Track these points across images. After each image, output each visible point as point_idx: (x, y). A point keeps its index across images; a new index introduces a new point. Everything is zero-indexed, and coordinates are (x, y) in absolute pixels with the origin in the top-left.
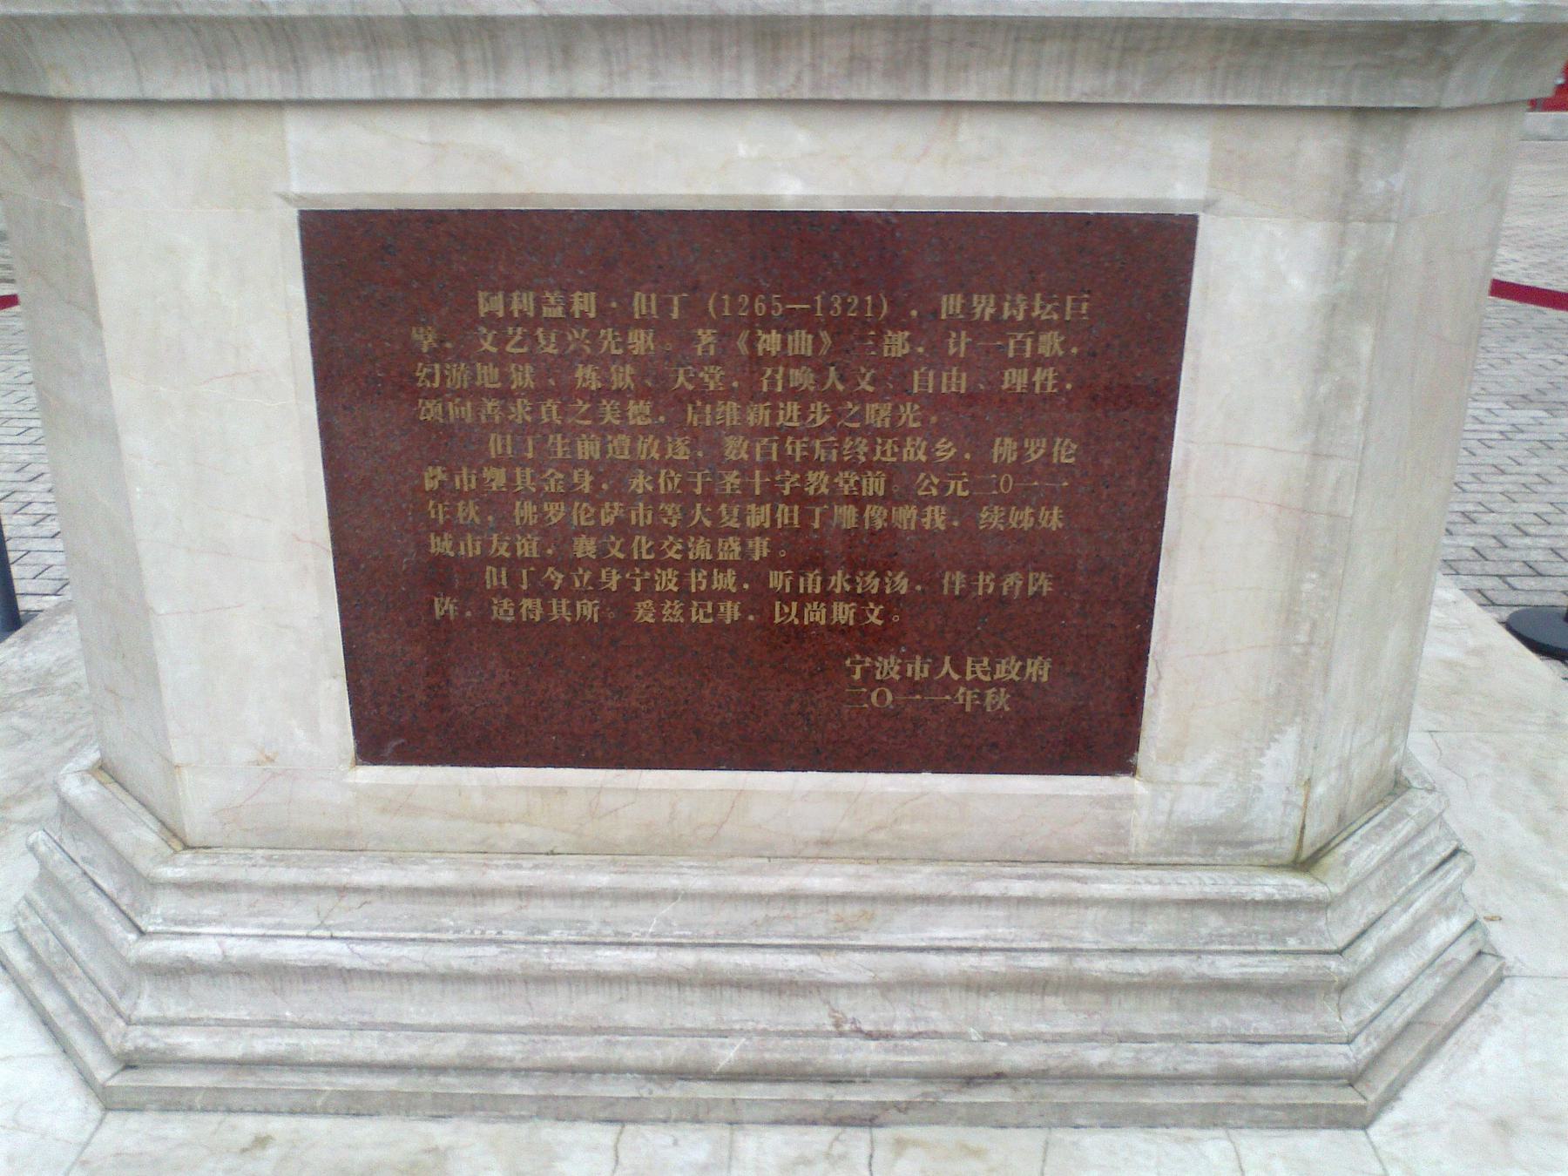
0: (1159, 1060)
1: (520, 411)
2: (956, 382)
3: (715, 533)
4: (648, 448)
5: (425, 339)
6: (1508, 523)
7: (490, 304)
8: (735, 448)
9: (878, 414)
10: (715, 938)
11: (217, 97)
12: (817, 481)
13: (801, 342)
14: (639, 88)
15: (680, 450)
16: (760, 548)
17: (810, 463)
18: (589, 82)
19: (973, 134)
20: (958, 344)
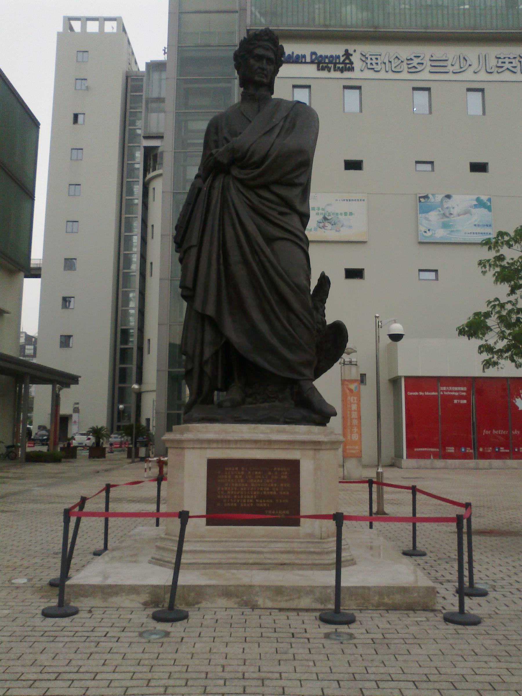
0: (304, 562)
1: (229, 481)
2: (276, 477)
3: (250, 495)
4: (243, 485)
5: (219, 472)
6: (469, 661)
7: (227, 469)
8: (253, 485)
9: (268, 481)
10: (250, 26)
11: (156, 501)
12: (261, 489)
13: (260, 473)
14: (243, 446)
15: (246, 485)
16: (255, 497)
17: (260, 487)
18: (238, 446)
19: (277, 451)
20: (276, 473)
